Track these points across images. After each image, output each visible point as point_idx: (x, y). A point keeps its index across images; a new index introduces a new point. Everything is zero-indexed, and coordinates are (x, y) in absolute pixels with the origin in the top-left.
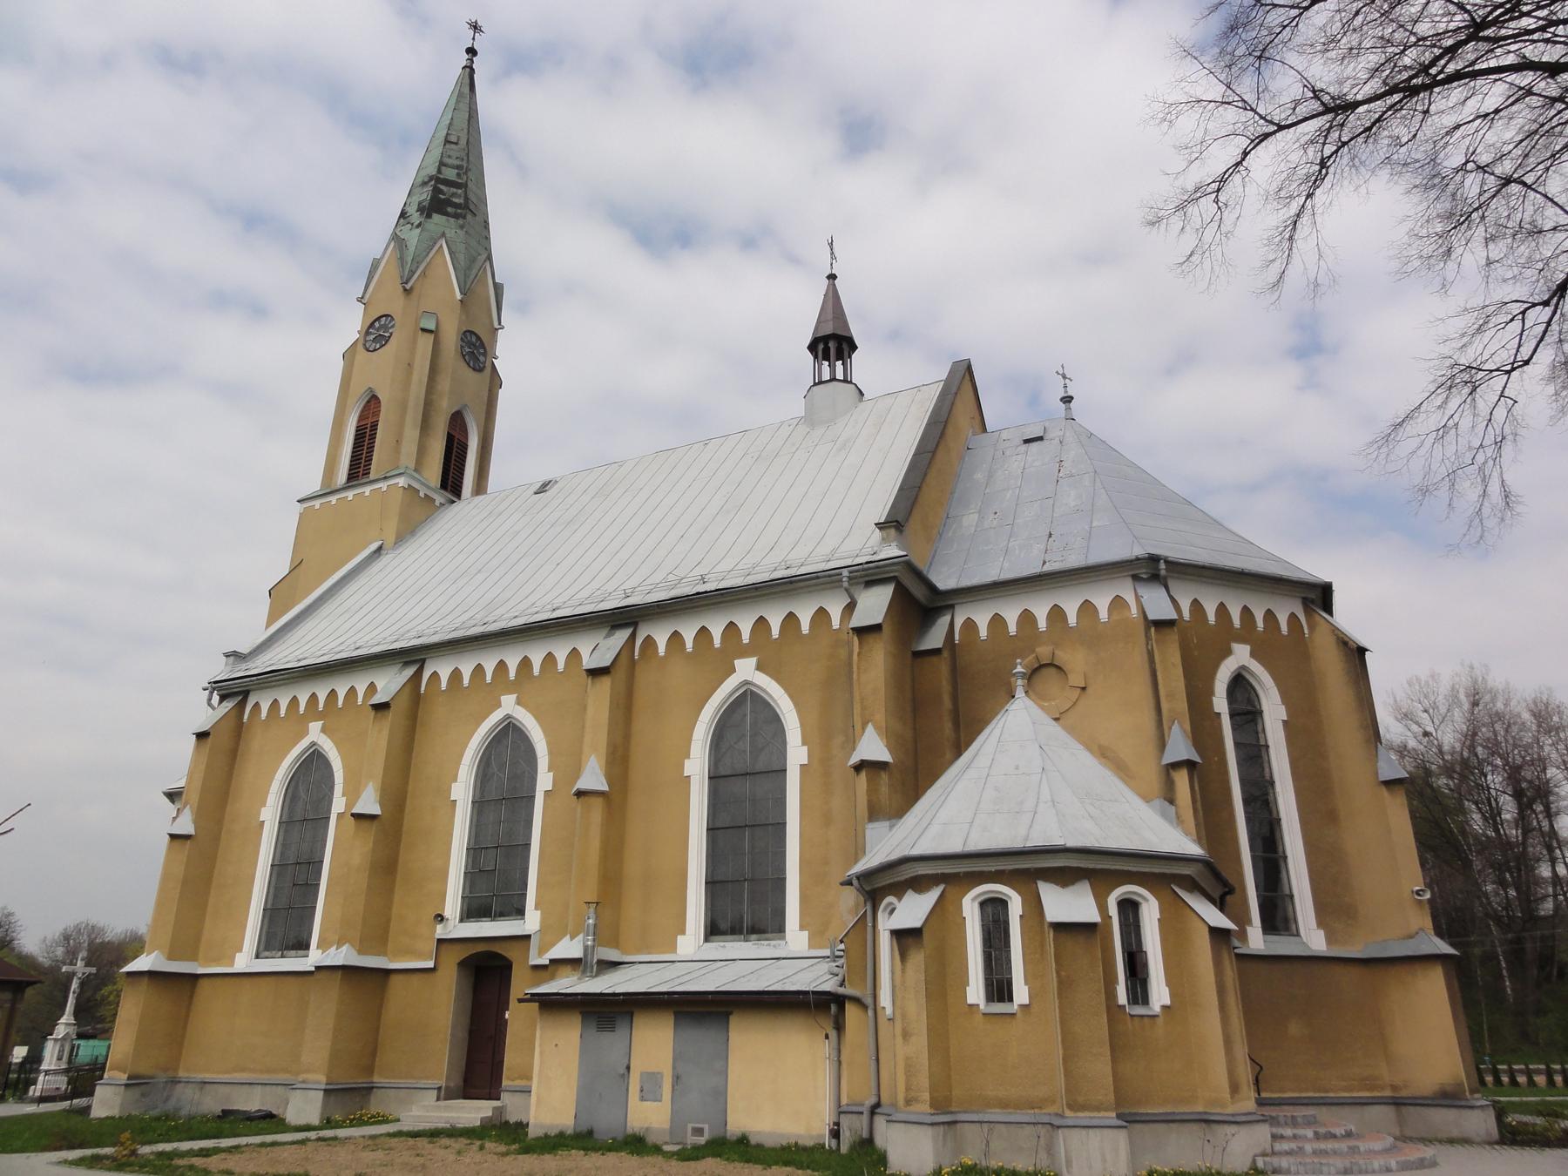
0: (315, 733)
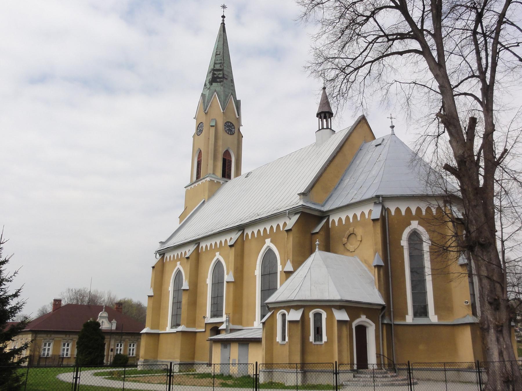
0: (218, 256)
